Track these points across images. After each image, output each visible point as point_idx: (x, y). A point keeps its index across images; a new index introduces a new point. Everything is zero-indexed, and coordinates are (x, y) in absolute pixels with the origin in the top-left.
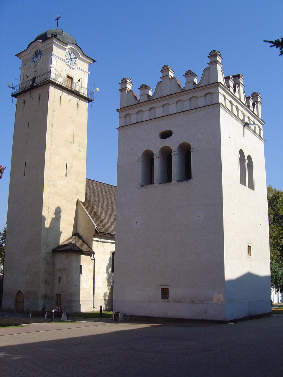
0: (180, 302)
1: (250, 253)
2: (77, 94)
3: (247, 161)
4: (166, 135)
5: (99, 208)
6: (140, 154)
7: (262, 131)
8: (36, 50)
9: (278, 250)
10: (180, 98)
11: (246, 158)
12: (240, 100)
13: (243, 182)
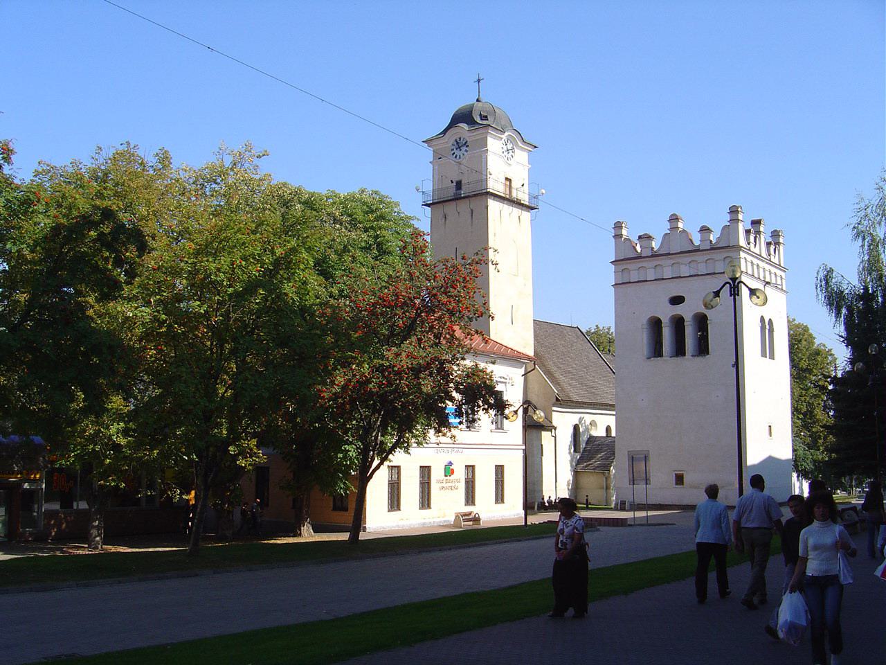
0: (695, 488)
1: (495, 236)
2: (518, 203)
3: (767, 327)
4: (677, 300)
5: (551, 363)
6: (644, 320)
7: (784, 281)
8: (457, 137)
9: (798, 418)
10: (693, 258)
11: (767, 323)
12: (760, 256)
13: (764, 355)
